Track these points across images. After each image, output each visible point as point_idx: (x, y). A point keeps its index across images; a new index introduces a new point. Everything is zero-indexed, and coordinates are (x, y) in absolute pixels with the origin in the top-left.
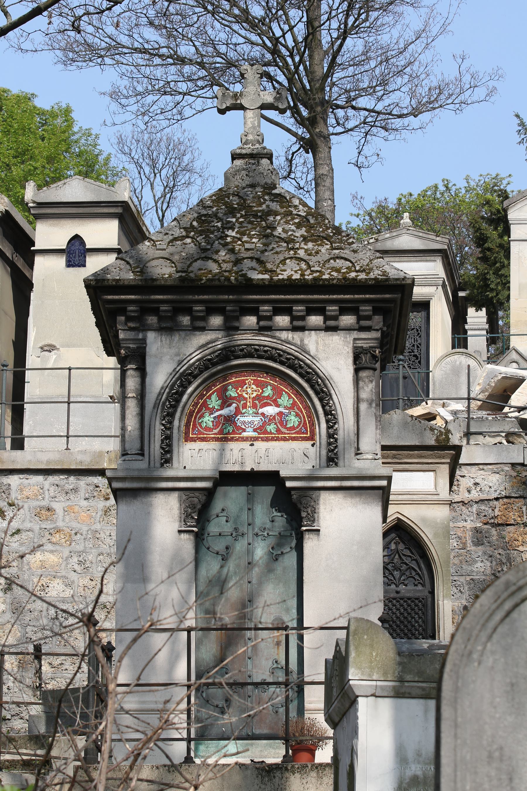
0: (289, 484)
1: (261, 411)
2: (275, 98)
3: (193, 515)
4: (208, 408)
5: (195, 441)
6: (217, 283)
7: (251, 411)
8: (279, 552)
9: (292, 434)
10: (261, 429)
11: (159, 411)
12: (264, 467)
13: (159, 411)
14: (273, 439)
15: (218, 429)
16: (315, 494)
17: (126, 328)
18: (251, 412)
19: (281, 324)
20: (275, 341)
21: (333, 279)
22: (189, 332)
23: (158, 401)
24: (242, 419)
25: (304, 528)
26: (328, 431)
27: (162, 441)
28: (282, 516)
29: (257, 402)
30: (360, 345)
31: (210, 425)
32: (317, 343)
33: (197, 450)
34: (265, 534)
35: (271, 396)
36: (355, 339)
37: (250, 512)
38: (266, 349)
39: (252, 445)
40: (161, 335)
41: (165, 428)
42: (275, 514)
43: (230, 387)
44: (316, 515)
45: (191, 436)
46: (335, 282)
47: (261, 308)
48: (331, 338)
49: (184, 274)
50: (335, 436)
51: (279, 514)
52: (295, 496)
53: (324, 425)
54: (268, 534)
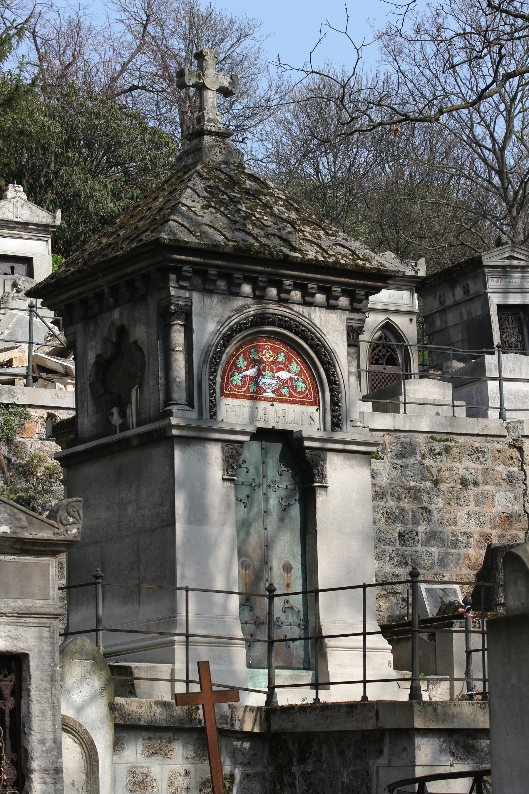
0: (307, 444)
1: (277, 374)
2: (229, 83)
3: (233, 465)
4: (237, 368)
5: (228, 397)
6: (262, 255)
7: (270, 374)
10: (276, 392)
11: (208, 367)
12: (280, 426)
14: (286, 402)
15: (245, 388)
16: (322, 454)
17: (177, 286)
18: (269, 375)
19: (295, 298)
20: (293, 313)
21: (348, 265)
22: (225, 296)
24: (263, 380)
25: (317, 484)
28: (288, 471)
31: (239, 383)
32: (321, 319)
33: (231, 406)
34: (276, 486)
36: (348, 319)
37: (264, 465)
38: (287, 319)
39: (272, 405)
40: (204, 296)
42: (283, 468)
43: (253, 350)
46: (349, 267)
47: (285, 282)
48: (330, 315)
49: (236, 244)
51: (286, 469)
52: (308, 454)
53: (328, 394)
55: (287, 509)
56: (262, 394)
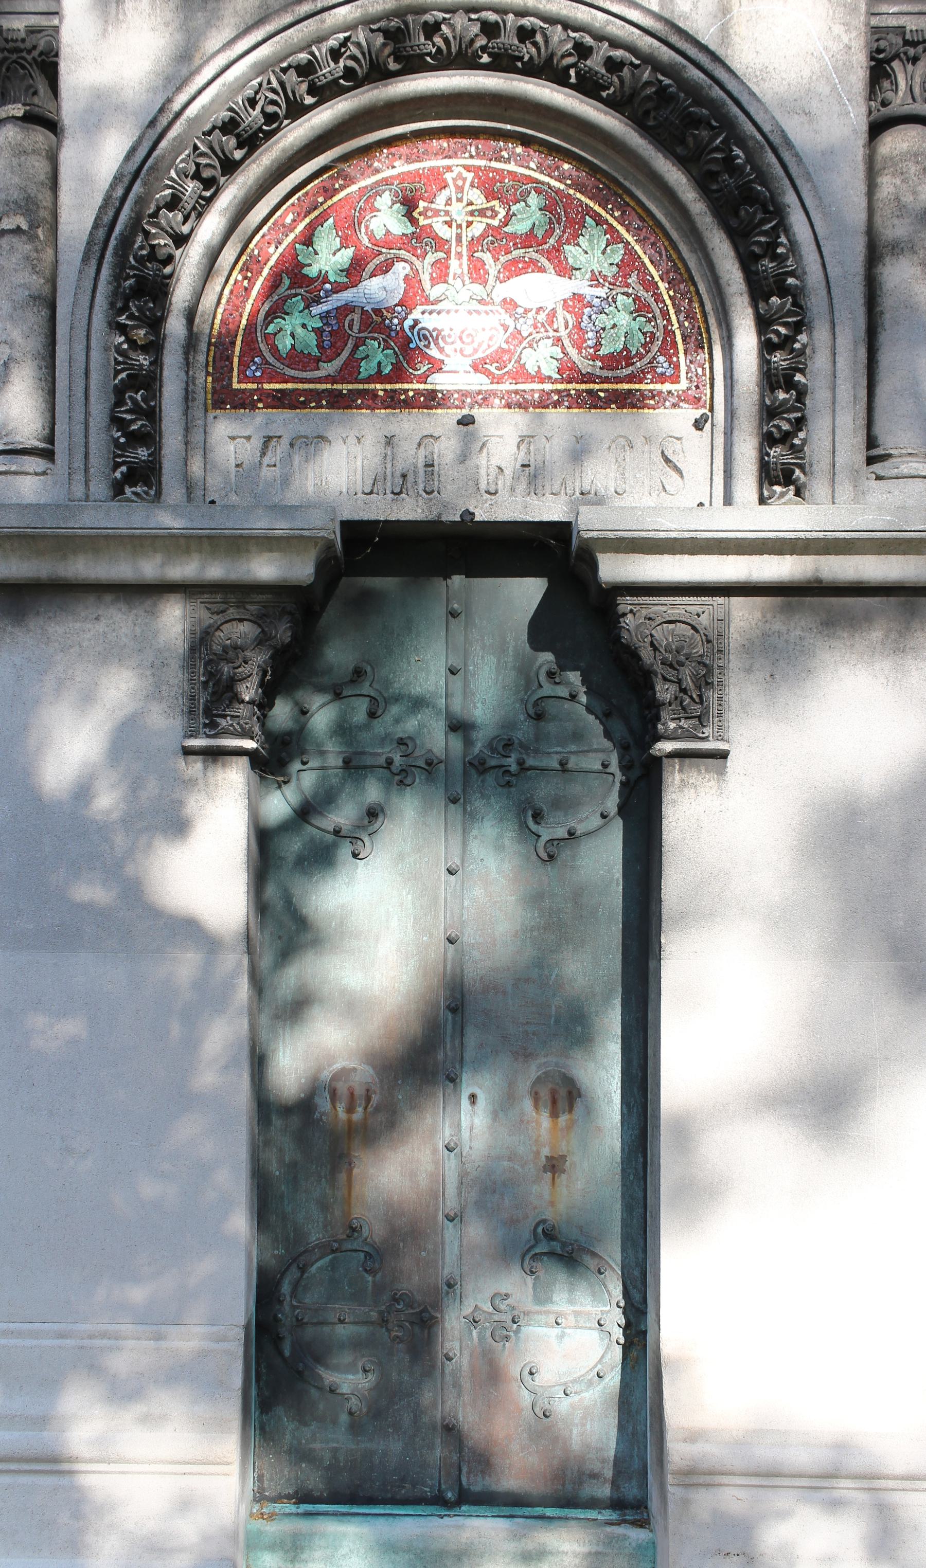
1: (503, 291)
8: (562, 833)
9: (619, 380)
11: (105, 272)
13: (105, 272)
15: (338, 363)
18: (464, 295)
23: (101, 233)
25: (667, 746)
26: (764, 362)
27: (119, 392)
29: (487, 257)
30: (893, 22)
35: (540, 234)
41: (129, 341)
44: (711, 696)
45: (236, 386)
50: (798, 377)
54: (521, 763)
55: (565, 855)
56: (423, 379)
